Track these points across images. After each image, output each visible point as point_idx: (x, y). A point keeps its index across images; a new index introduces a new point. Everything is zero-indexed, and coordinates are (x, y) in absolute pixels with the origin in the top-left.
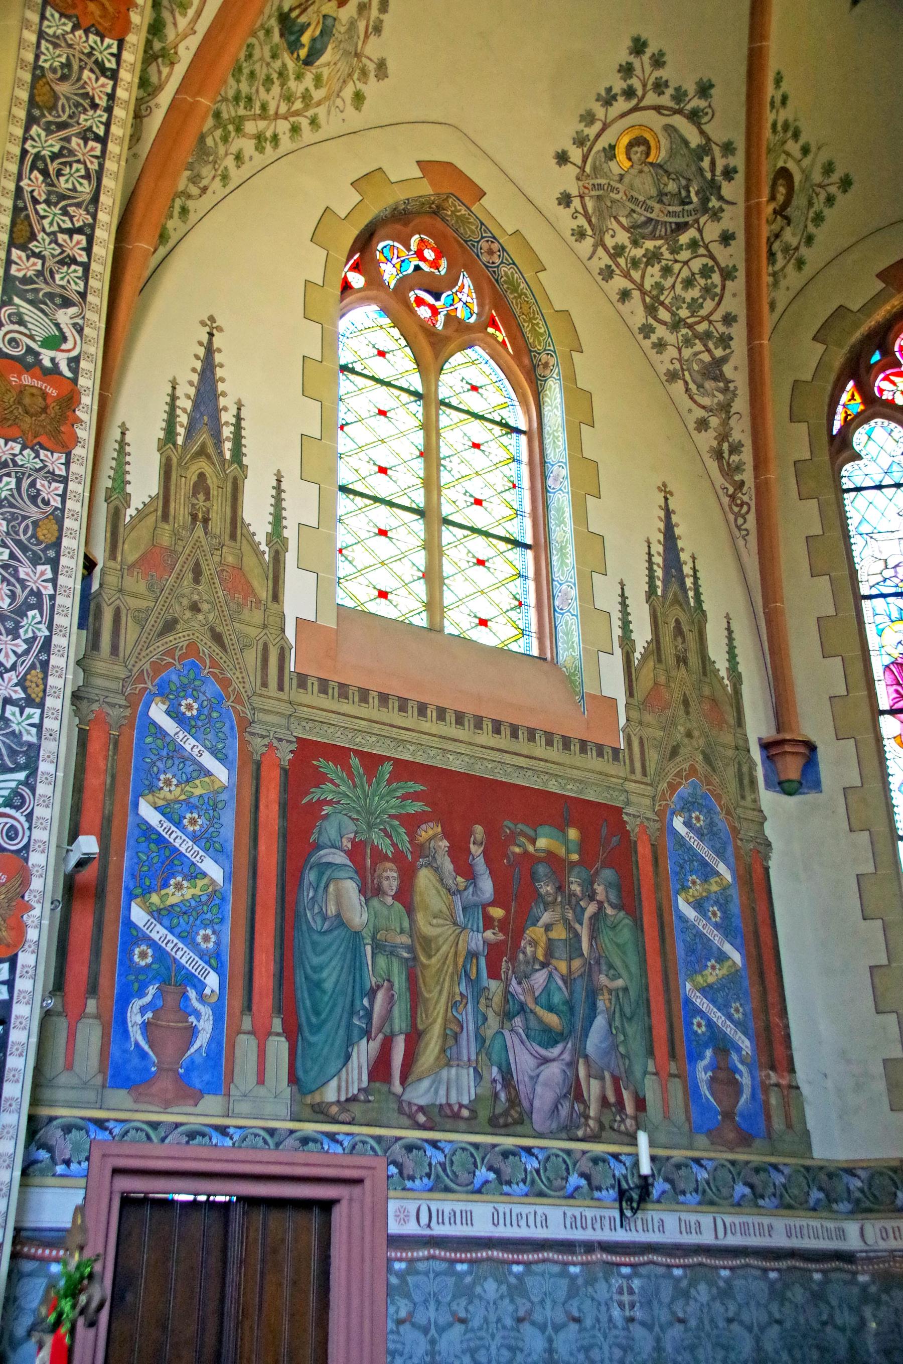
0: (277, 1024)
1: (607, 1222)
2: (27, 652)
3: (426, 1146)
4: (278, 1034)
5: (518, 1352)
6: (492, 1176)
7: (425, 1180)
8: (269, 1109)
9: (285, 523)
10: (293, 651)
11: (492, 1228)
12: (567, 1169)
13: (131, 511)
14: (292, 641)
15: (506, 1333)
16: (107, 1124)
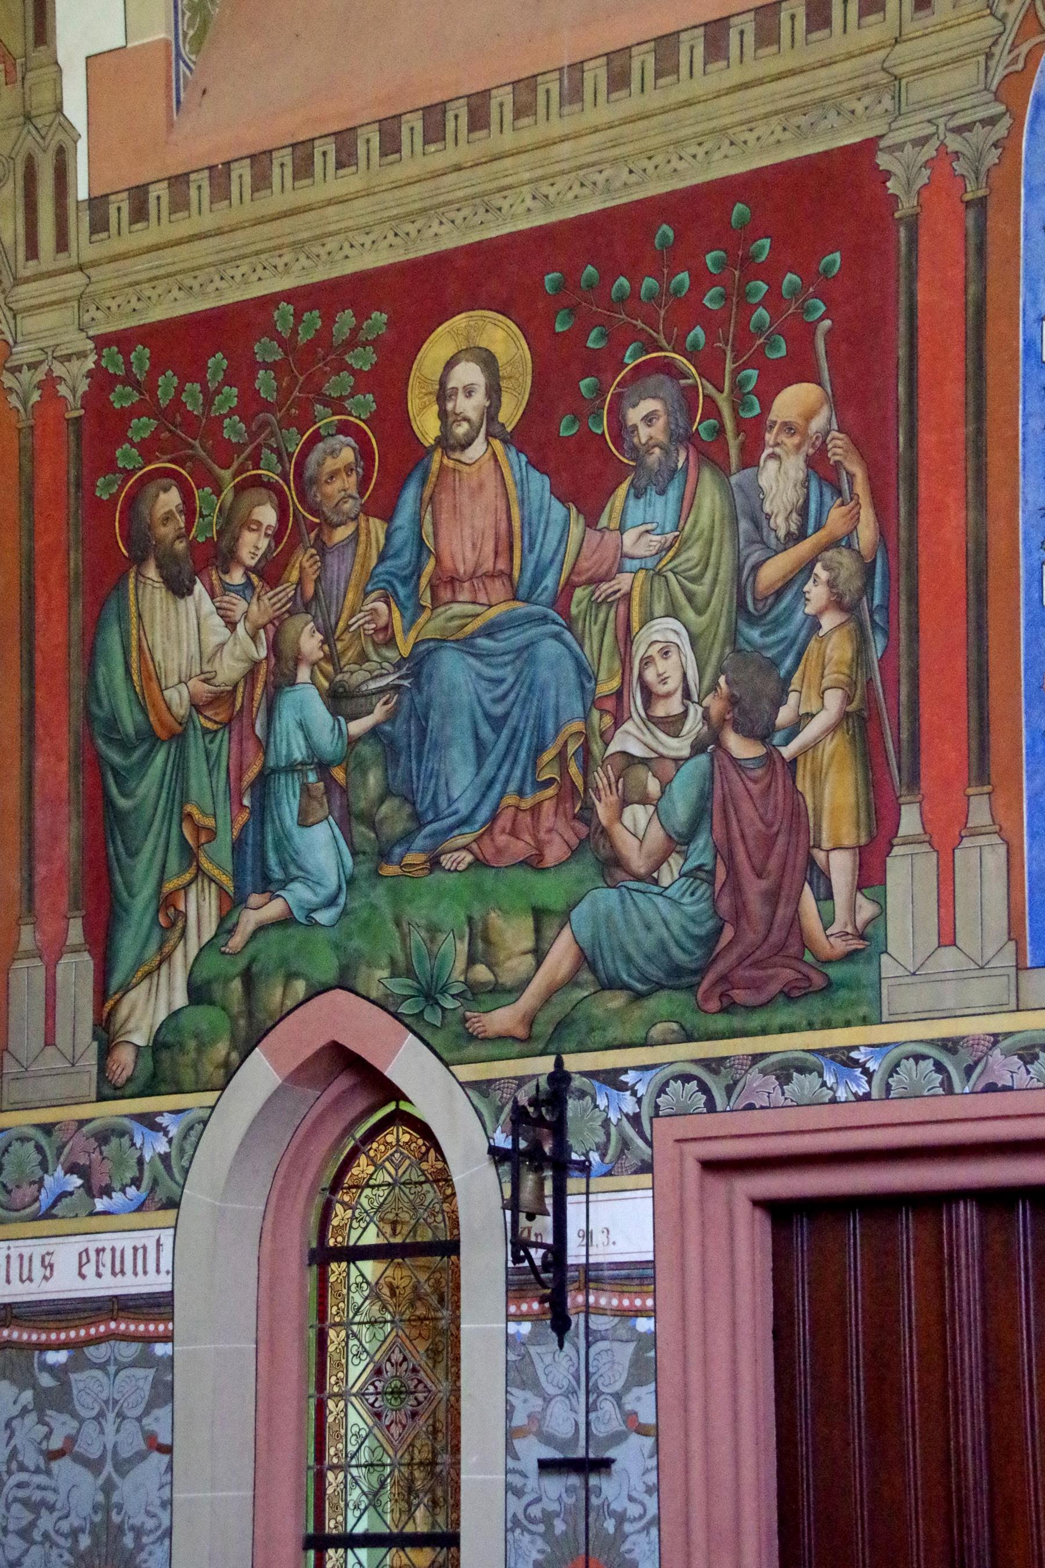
0: (76, 933)
1: (107, 1257)
4: (75, 950)
5: (44, 1512)
7: (132, 1191)
8: (53, 1088)
10: (82, 146)
11: (79, 1283)
15: (23, 1477)
16: (623, 1078)
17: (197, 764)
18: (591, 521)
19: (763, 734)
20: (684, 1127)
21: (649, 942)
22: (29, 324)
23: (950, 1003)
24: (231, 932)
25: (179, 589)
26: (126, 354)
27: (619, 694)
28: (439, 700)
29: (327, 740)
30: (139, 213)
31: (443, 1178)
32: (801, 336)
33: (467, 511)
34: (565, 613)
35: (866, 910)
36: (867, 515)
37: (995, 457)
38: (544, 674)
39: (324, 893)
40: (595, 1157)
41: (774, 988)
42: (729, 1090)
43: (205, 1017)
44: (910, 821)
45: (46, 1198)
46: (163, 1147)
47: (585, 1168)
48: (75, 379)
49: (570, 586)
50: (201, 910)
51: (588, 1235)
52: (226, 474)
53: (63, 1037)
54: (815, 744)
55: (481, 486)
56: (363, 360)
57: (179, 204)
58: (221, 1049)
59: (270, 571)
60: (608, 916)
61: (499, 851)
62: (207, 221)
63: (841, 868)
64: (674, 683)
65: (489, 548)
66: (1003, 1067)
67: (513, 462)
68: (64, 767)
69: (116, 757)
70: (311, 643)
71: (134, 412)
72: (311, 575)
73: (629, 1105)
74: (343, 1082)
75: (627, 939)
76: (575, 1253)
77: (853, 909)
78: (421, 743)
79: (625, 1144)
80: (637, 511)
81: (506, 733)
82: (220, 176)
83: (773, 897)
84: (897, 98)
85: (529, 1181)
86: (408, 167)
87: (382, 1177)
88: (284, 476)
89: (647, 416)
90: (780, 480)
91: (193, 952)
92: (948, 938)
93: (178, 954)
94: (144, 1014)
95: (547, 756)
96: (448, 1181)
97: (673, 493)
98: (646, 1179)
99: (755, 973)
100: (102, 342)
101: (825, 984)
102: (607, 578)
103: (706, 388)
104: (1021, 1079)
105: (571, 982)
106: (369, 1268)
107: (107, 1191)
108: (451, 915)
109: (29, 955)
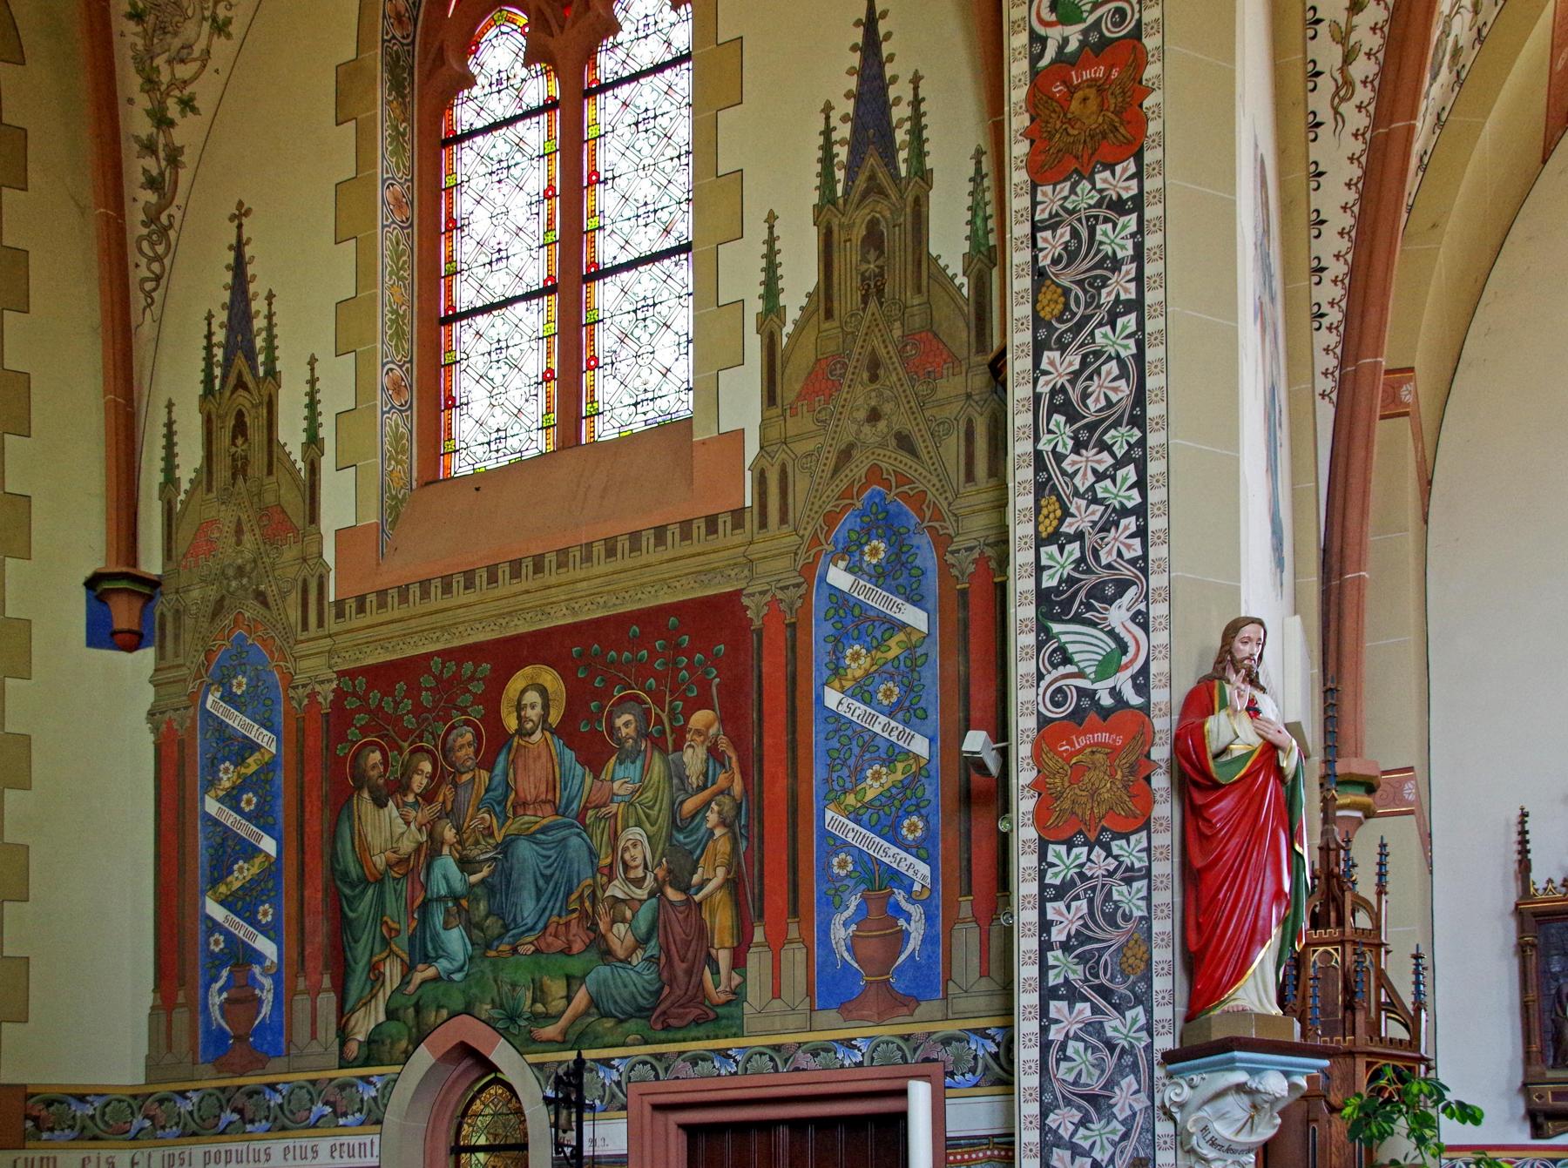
0: (327, 982)
2: (1125, 1137)
3: (359, 1082)
4: (326, 991)
6: (236, 1117)
7: (357, 1115)
9: (781, 284)
10: (332, 574)
12: (132, 1113)
13: (789, 328)
14: (332, 564)
17: (390, 898)
18: (596, 776)
19: (685, 888)
20: (644, 1087)
21: (626, 995)
22: (304, 664)
23: (778, 1026)
24: (408, 983)
25: (380, 803)
26: (353, 680)
27: (611, 866)
28: (516, 866)
29: (458, 886)
30: (361, 609)
31: (519, 1112)
32: (704, 685)
33: (532, 766)
34: (583, 822)
35: (736, 979)
36: (738, 778)
37: (801, 752)
38: (572, 854)
39: (457, 965)
40: (597, 1102)
41: (691, 1017)
42: (666, 1070)
43: (394, 1027)
44: (759, 935)
45: (313, 1118)
46: (373, 1093)
47: (592, 1108)
48: (326, 692)
49: (586, 809)
50: (392, 972)
51: (594, 1141)
52: (406, 745)
53: (321, 1034)
54: (711, 895)
55: (539, 756)
56: (478, 688)
57: (382, 605)
58: (404, 1044)
59: (428, 796)
60: (605, 980)
61: (549, 945)
62: (396, 614)
63: (724, 958)
64: (639, 861)
65: (543, 788)
66: (803, 1060)
67: (556, 744)
68: (320, 895)
69: (347, 891)
70: (449, 834)
71: (358, 710)
72: (450, 797)
73: (616, 1077)
74: (467, 1062)
75: (614, 992)
76: (587, 1150)
77: (730, 979)
78: (508, 886)
79: (613, 1096)
80: (620, 772)
81: (552, 884)
82: (404, 592)
83: (689, 973)
84: (751, 570)
85: (564, 1113)
86: (501, 591)
87: (488, 1111)
88: (436, 746)
89: (625, 723)
90: (693, 759)
91: (388, 993)
92: (777, 994)
93: (381, 994)
94: (364, 1024)
95: (573, 897)
96: (522, 1114)
97: (639, 763)
98: (624, 1113)
99: (681, 1010)
100: (341, 674)
101: (718, 1017)
102: (605, 805)
103: (654, 710)
104: (812, 1065)
105: (586, 1013)
106: (481, 1156)
107: (345, 1115)
108: (523, 978)
109: (302, 993)
